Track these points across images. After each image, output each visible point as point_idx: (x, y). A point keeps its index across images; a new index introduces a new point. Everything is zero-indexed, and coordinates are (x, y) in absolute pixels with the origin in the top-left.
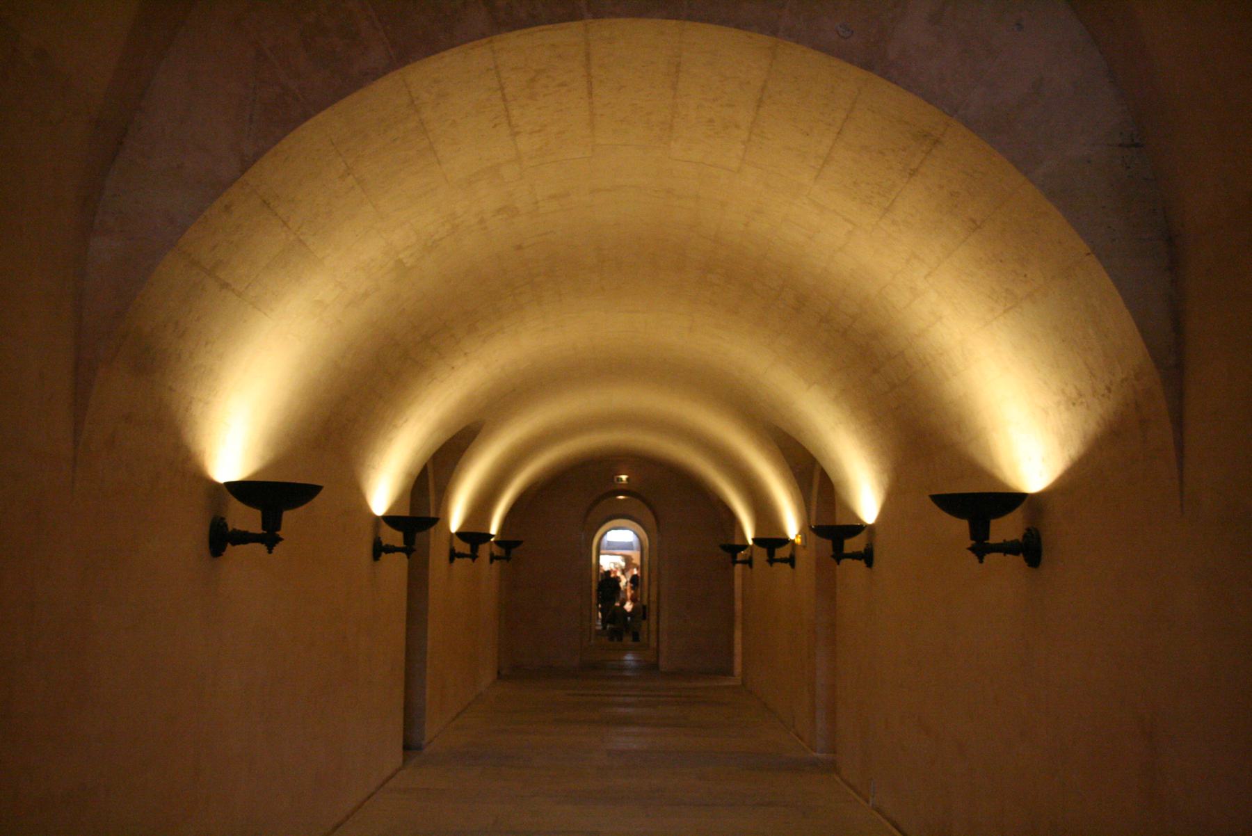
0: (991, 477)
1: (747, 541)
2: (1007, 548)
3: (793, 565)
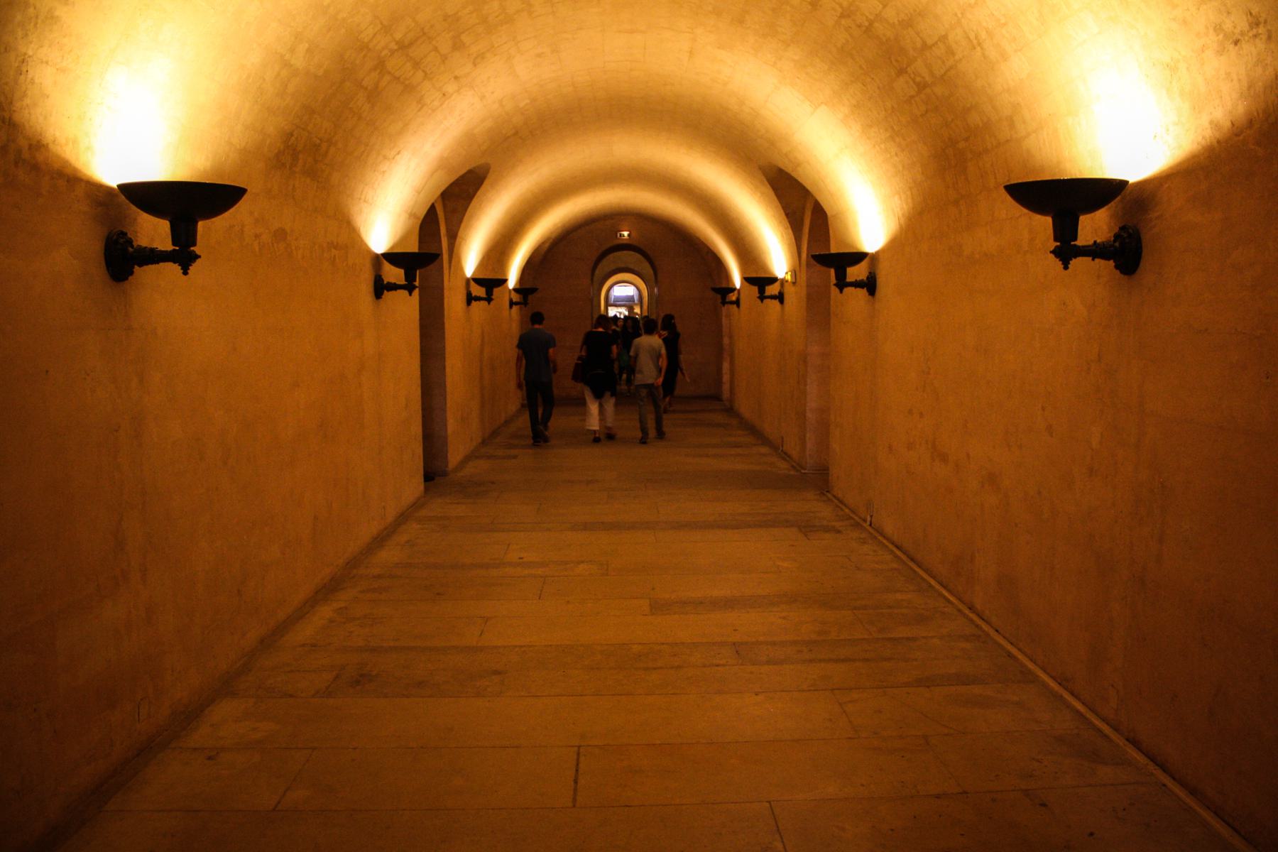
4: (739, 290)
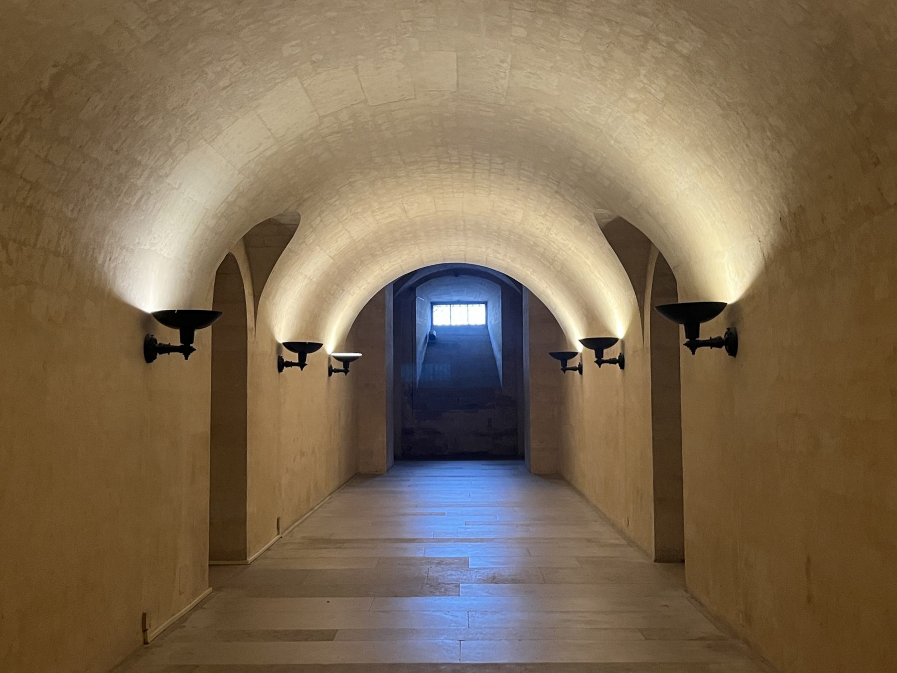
0: (610, 332)
1: (571, 345)
2: (714, 343)
3: (622, 366)
4: (581, 354)
